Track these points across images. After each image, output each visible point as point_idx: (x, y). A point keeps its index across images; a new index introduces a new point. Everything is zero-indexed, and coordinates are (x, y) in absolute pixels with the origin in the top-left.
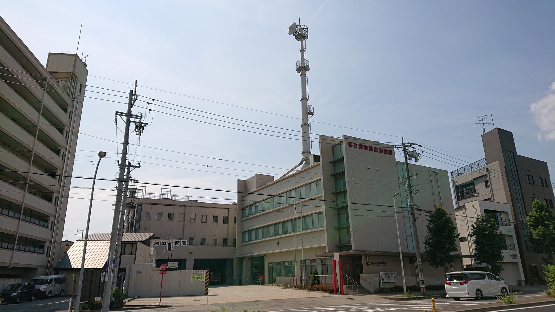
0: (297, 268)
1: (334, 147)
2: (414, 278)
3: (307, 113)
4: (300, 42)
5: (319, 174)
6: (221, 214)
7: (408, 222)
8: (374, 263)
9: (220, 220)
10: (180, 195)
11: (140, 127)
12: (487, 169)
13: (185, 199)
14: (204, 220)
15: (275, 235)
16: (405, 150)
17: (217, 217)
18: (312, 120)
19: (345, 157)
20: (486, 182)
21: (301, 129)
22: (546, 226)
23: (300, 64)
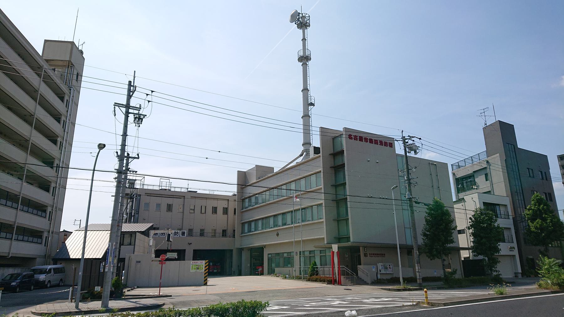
0: (296, 258)
4: (301, 31)
6: (221, 206)
8: (372, 255)
9: (220, 211)
10: (179, 186)
12: (488, 162)
14: (203, 211)
15: (274, 227)
18: (313, 111)
20: (486, 175)
21: (301, 121)
22: (544, 220)
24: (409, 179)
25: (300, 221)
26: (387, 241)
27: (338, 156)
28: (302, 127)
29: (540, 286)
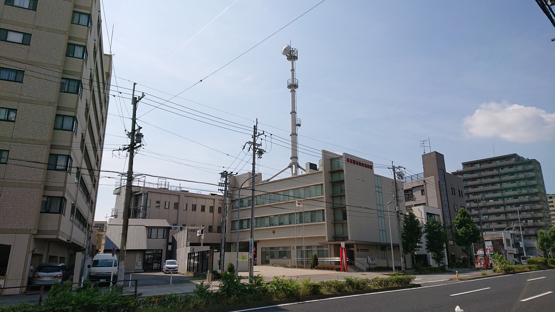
0: (294, 252)
1: (332, 160)
2: (385, 261)
3: (296, 125)
4: (291, 62)
5: (322, 180)
6: (208, 204)
7: (396, 221)
8: (362, 250)
9: (207, 209)
10: (174, 185)
11: (261, 152)
12: (424, 181)
13: (178, 190)
14: (167, 207)
15: (270, 225)
16: (394, 170)
17: (204, 206)
18: (299, 130)
19: (344, 170)
20: (422, 191)
21: (290, 138)
22: (468, 227)
23: (290, 82)
24: (397, 197)
25: (298, 222)
26: (384, 241)
27: (337, 173)
28: (290, 143)
29: (494, 271)
